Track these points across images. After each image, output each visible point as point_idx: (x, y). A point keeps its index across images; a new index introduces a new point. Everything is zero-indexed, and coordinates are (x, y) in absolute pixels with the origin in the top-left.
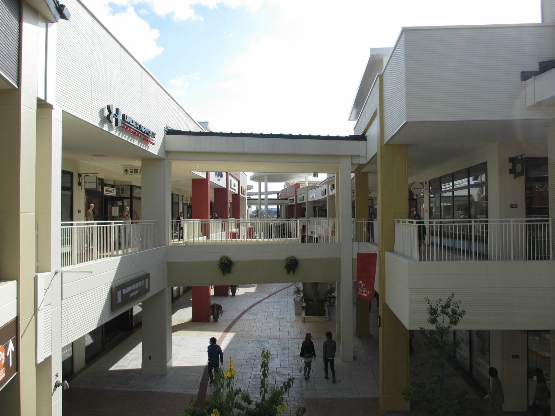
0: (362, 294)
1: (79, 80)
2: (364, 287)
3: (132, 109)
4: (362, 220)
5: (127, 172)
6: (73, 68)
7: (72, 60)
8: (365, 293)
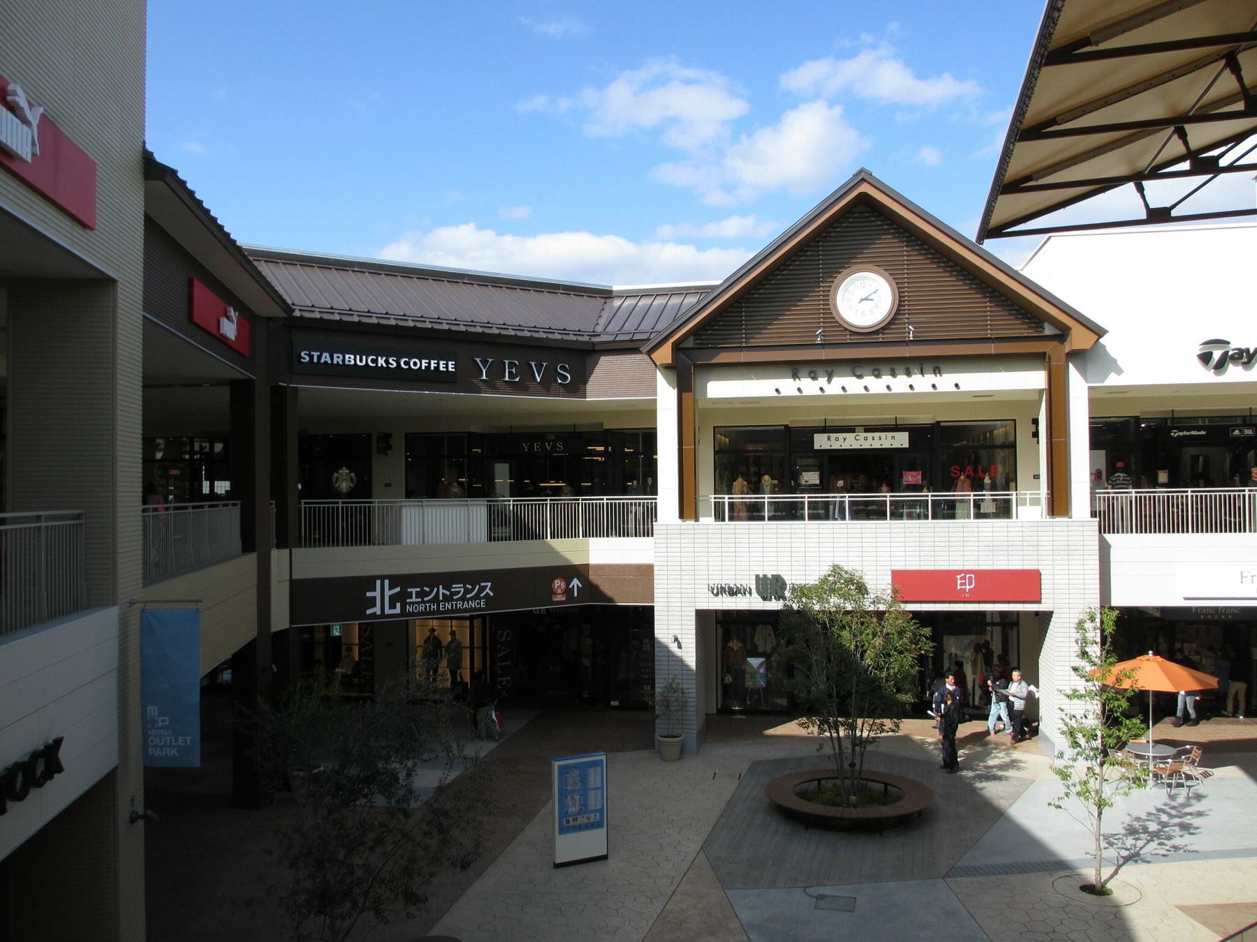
0: (158, 752)
2: (164, 727)
4: (338, 503)
8: (171, 746)
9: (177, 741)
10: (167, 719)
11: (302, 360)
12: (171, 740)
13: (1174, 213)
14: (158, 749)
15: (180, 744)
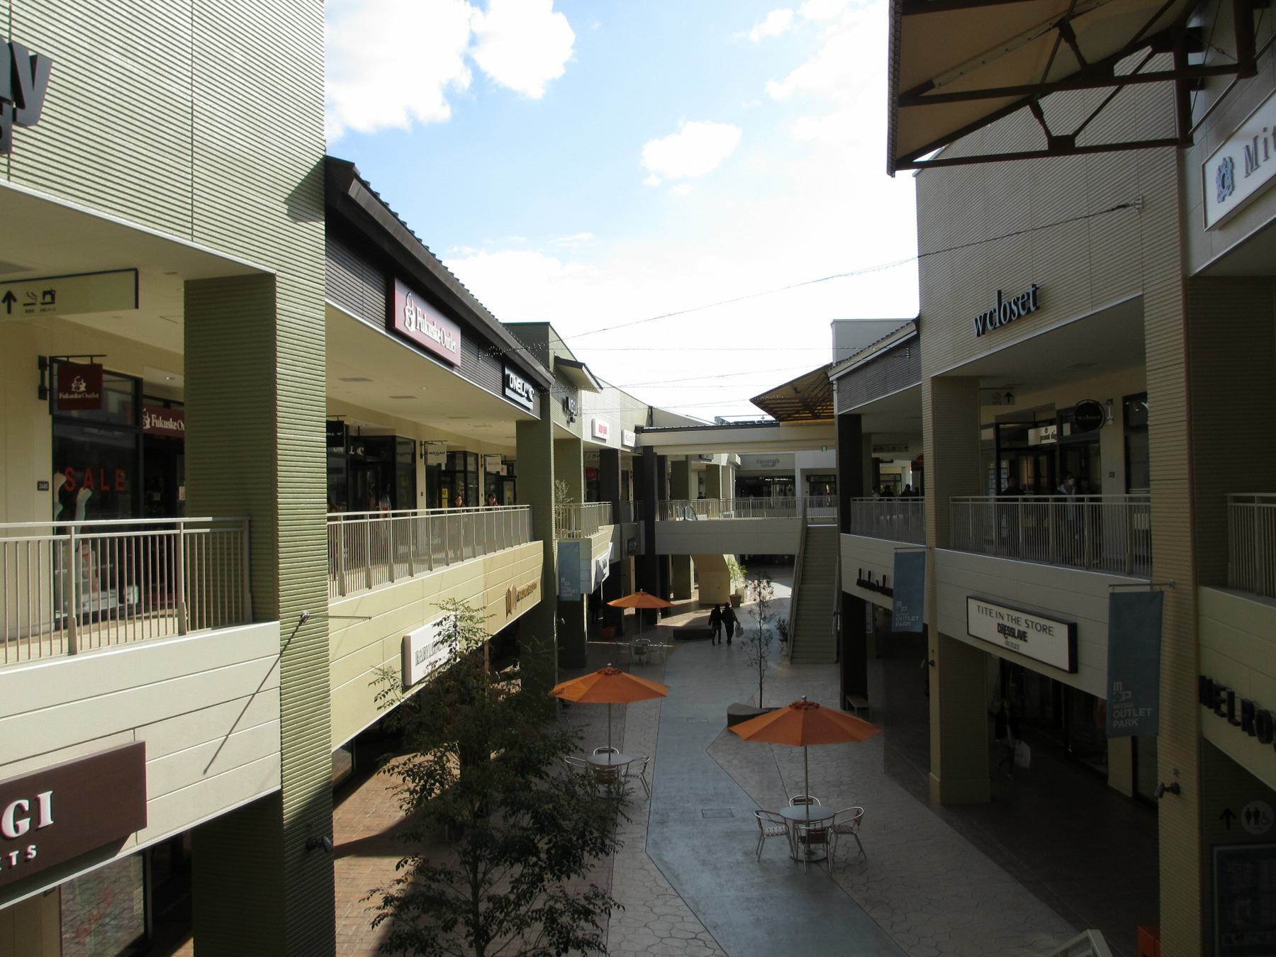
1: (171, 219)
3: (1081, 272)
5: (13, 303)
6: (177, 19)
7: (239, 29)
9: (1137, 712)
10: (1130, 693)
11: (78, 377)
12: (1132, 712)
13: (1080, 142)
14: (1122, 721)
15: (1141, 715)
